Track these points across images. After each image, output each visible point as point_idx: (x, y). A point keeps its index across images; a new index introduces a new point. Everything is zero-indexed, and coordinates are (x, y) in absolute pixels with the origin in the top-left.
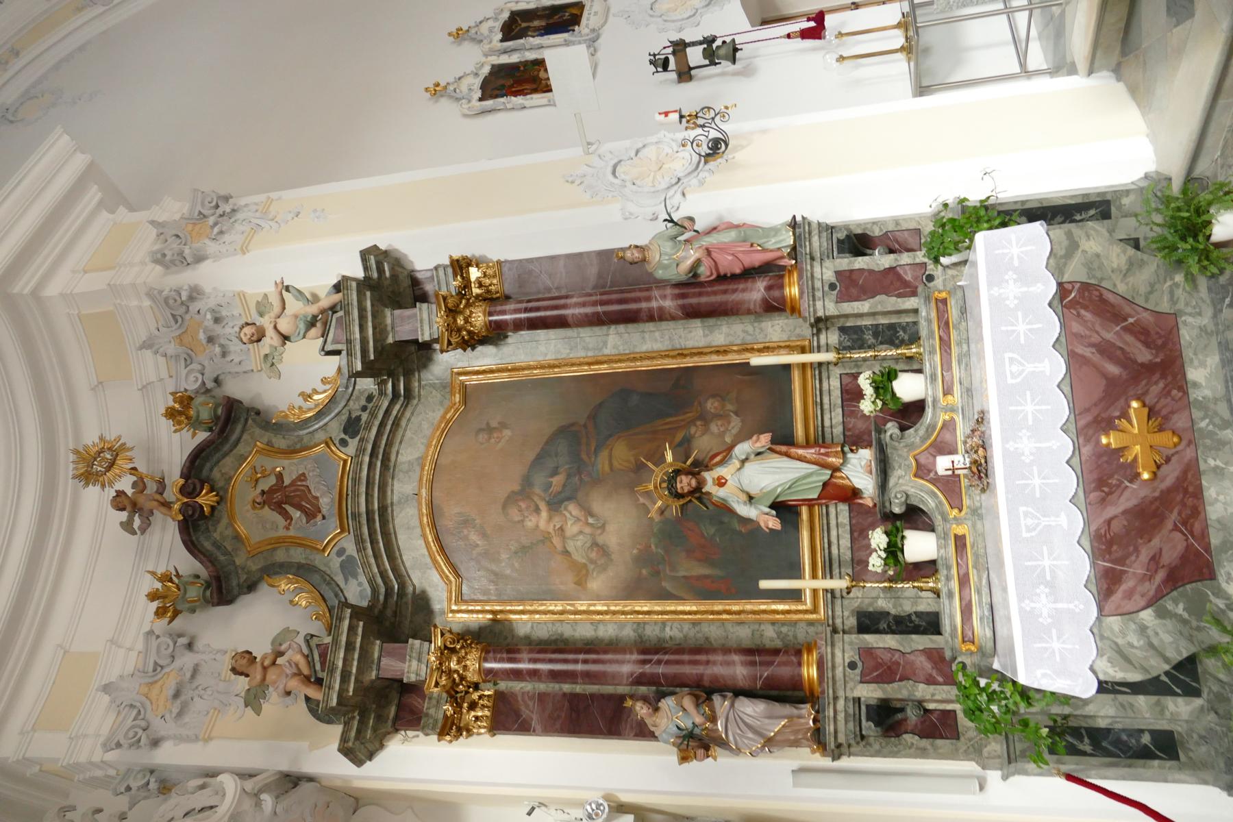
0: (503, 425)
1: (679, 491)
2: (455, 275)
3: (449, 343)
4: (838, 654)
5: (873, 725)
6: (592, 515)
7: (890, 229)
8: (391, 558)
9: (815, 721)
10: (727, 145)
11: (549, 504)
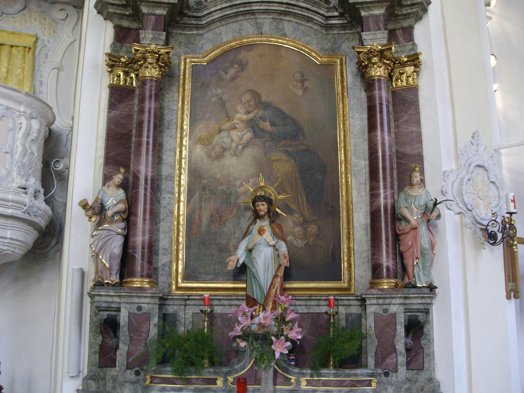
0: (305, 90)
1: (257, 203)
2: (408, 57)
3: (359, 53)
4: (147, 300)
5: (105, 318)
6: (244, 148)
7: (425, 351)
8: (221, 19)
9: (108, 283)
10: (492, 244)
11: (252, 120)
